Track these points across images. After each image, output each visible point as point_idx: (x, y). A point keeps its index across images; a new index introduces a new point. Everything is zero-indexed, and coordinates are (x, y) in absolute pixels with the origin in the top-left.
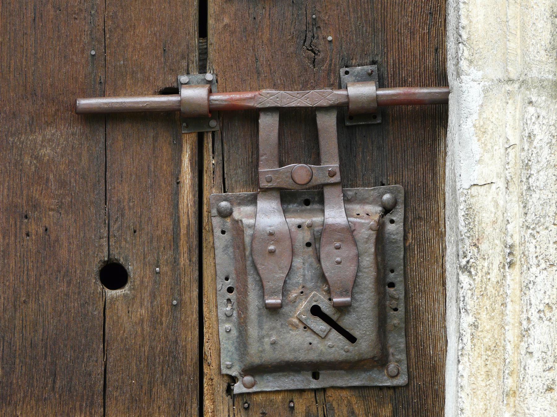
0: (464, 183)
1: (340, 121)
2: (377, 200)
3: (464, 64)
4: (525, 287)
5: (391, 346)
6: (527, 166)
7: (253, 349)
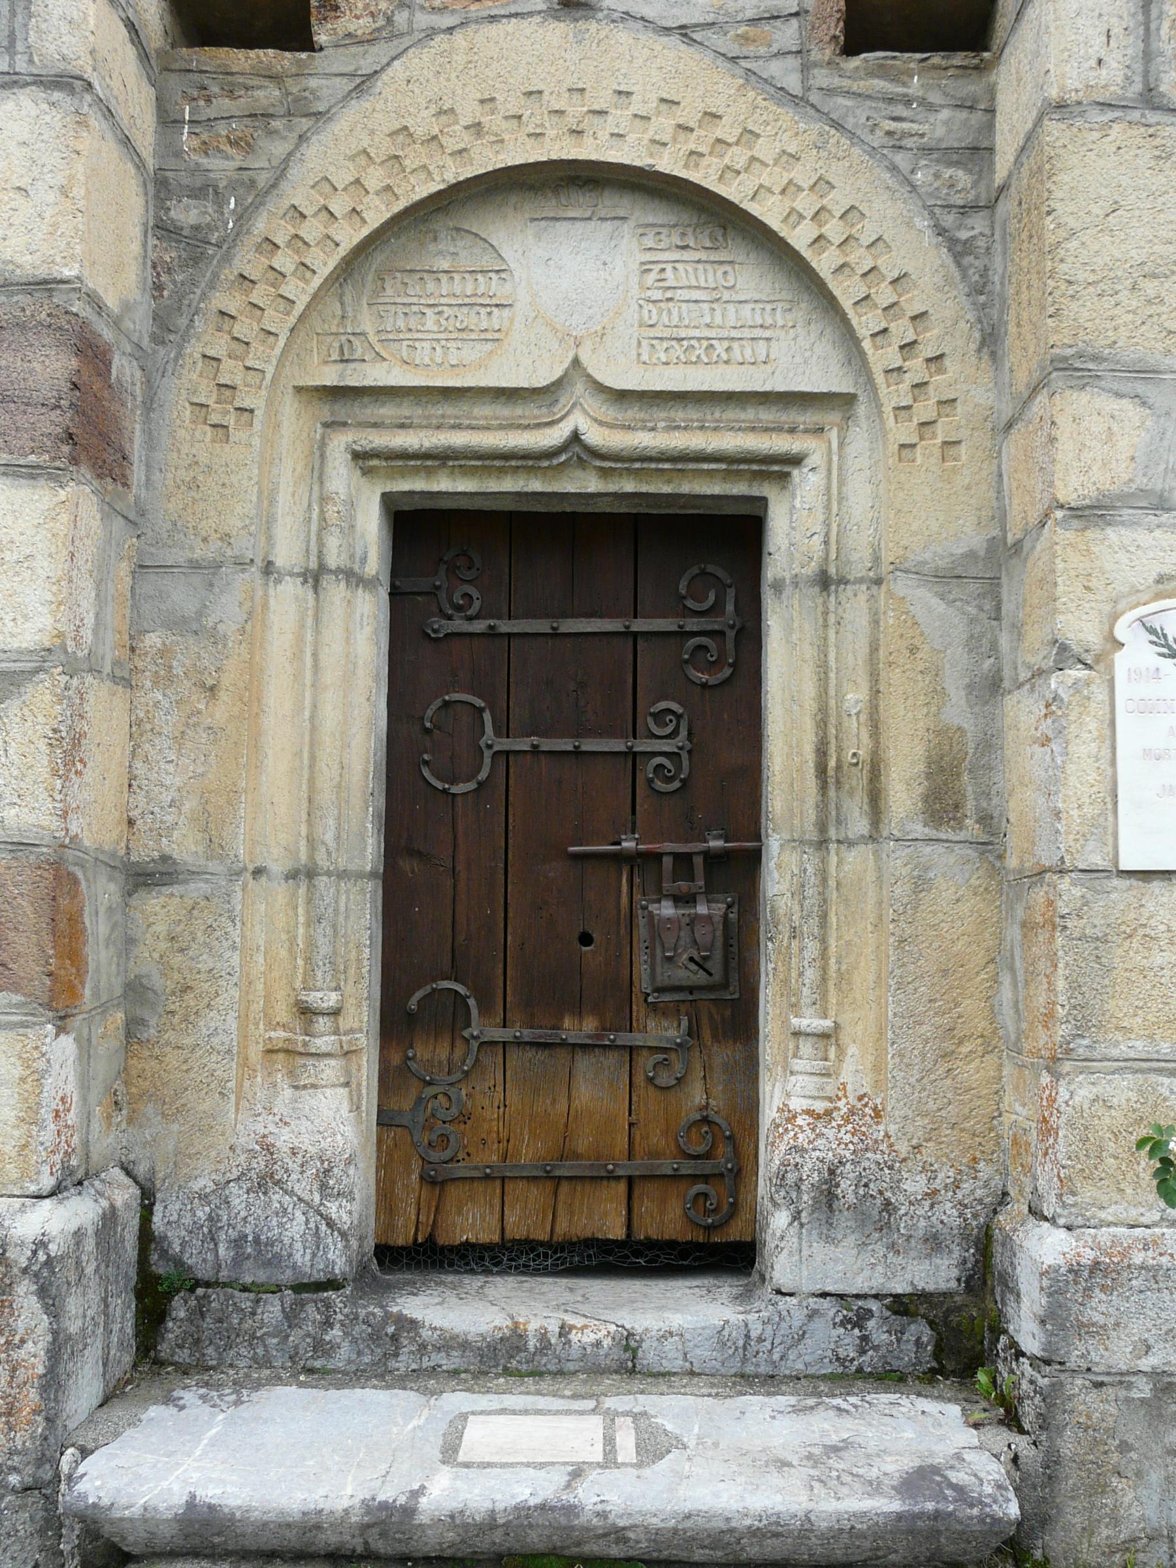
0: (770, 894)
1: (705, 860)
2: (724, 901)
3: (770, 831)
4: (801, 950)
5: (507, 1381)
6: (803, 886)
7: (659, 978)
